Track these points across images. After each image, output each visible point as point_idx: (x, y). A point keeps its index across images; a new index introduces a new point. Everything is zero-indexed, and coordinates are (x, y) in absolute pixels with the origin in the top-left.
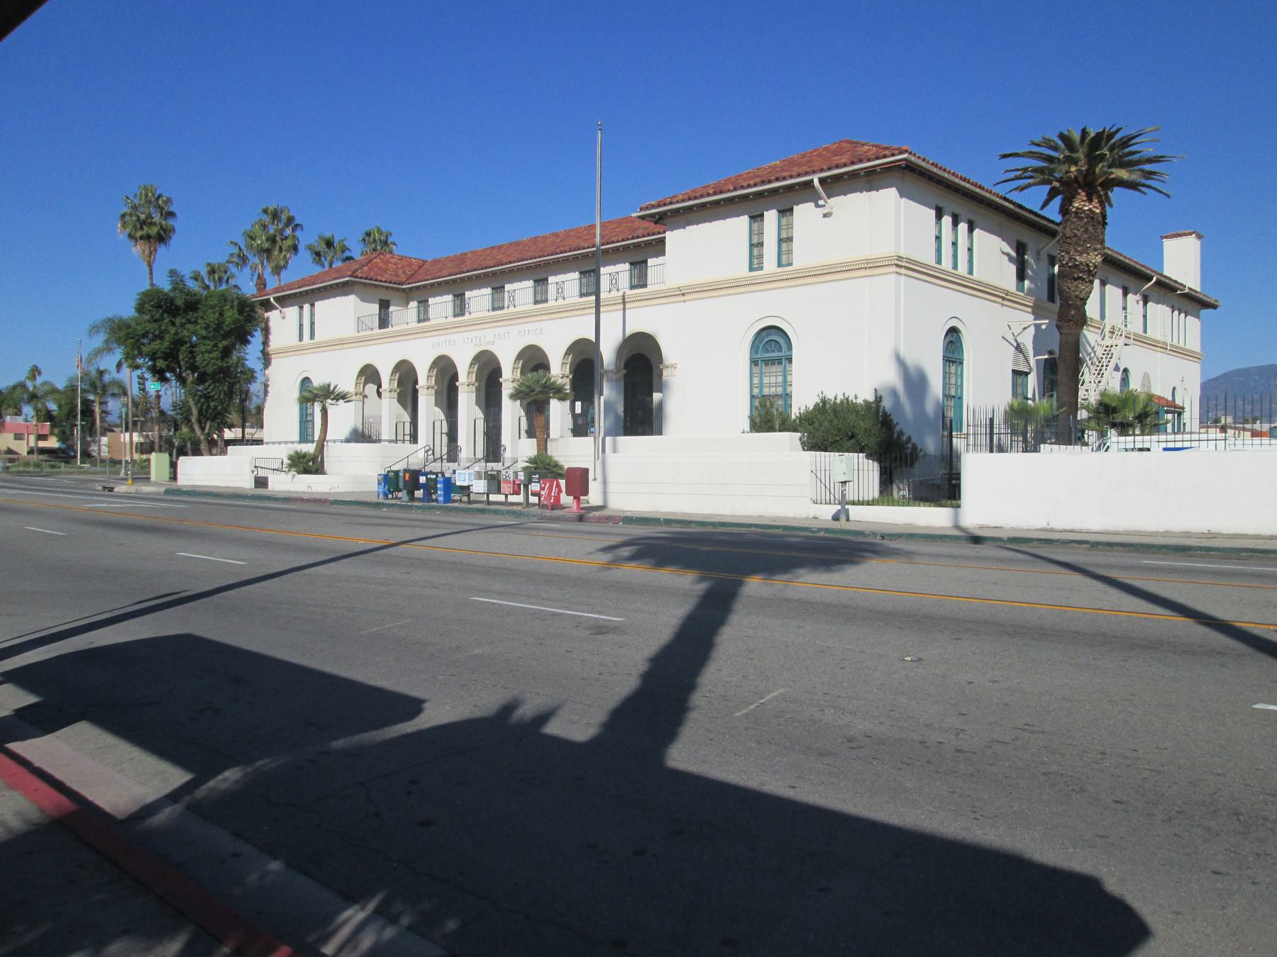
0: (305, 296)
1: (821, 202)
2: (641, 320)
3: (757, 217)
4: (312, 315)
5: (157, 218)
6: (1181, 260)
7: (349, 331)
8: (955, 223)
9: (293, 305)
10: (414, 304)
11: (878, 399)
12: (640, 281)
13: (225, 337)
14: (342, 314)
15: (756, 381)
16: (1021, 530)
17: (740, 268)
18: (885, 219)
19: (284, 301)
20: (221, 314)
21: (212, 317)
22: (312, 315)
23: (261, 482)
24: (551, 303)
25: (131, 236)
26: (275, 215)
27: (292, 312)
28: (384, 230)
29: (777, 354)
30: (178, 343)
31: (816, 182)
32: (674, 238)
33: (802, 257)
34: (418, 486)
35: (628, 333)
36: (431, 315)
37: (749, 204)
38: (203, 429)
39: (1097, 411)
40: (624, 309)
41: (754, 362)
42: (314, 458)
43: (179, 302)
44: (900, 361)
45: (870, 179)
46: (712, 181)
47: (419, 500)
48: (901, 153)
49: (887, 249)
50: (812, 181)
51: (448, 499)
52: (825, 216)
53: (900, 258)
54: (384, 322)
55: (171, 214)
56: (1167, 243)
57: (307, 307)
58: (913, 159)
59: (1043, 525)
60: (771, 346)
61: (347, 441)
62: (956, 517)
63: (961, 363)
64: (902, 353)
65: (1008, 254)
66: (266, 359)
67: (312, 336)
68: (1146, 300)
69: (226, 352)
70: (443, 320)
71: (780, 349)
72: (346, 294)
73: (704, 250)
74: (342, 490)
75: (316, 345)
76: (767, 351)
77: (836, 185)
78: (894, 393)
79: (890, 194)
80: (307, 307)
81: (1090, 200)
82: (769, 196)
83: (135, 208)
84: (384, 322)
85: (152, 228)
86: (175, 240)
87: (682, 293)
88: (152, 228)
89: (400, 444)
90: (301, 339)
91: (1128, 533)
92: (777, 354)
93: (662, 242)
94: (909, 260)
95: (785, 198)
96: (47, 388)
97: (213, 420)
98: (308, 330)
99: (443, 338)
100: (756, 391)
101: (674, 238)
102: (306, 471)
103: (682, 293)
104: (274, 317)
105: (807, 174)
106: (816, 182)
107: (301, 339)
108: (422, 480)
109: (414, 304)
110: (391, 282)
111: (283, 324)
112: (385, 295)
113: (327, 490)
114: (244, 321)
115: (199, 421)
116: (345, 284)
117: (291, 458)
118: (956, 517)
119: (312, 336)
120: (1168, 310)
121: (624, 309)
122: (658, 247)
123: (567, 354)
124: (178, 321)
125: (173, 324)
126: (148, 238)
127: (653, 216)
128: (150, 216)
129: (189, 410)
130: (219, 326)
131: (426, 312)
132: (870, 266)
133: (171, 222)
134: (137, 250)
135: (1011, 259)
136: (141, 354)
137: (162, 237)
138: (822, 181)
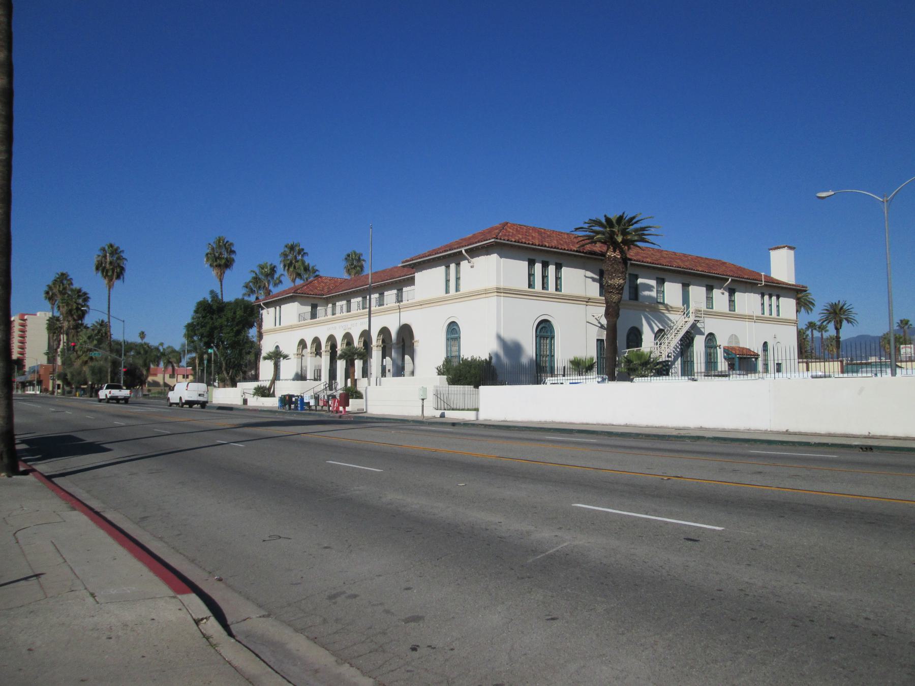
0: (277, 303)
2: (407, 317)
3: (448, 267)
4: (458, 272)
5: (225, 255)
6: (782, 266)
7: (294, 321)
8: (545, 265)
9: (441, 266)
10: (330, 305)
11: (491, 358)
12: (399, 299)
13: (237, 325)
14: (292, 311)
16: (562, 423)
17: (441, 293)
18: (487, 270)
19: (268, 305)
20: (235, 313)
21: (230, 315)
22: (458, 272)
23: (245, 401)
25: (211, 265)
26: (292, 248)
27: (272, 310)
28: (358, 252)
30: (213, 329)
32: (419, 276)
33: (464, 289)
34: (292, 403)
38: (228, 374)
39: (806, 357)
41: (447, 339)
42: (270, 388)
43: (215, 307)
44: (499, 338)
45: (486, 250)
46: (426, 251)
49: (493, 284)
51: (302, 409)
53: (498, 288)
54: (314, 315)
55: (234, 252)
56: (772, 253)
57: (453, 266)
59: (503, 419)
60: (453, 330)
61: (293, 380)
62: (477, 415)
63: (553, 337)
64: (503, 335)
65: (592, 278)
66: (260, 336)
67: (457, 290)
68: (732, 292)
69: (238, 333)
72: (294, 302)
73: (429, 281)
75: (285, 328)
77: (474, 252)
78: (497, 355)
79: (494, 257)
80: (453, 266)
81: (614, 251)
82: (449, 257)
83: (213, 249)
84: (314, 315)
85: (222, 258)
86: (235, 266)
87: (421, 304)
88: (222, 258)
90: (447, 291)
91: (830, 435)
93: (413, 279)
94: (504, 289)
95: (457, 258)
96: (170, 350)
97: (233, 368)
98: (278, 320)
99: (354, 322)
101: (419, 276)
102: (264, 395)
103: (421, 304)
104: (264, 312)
107: (447, 291)
108: (294, 399)
109: (330, 305)
110: (317, 295)
111: (268, 316)
112: (315, 302)
114: (248, 315)
115: (226, 369)
116: (291, 297)
117: (255, 389)
118: (477, 415)
119: (457, 290)
120: (757, 297)
122: (411, 281)
124: (215, 317)
125: (212, 319)
126: (219, 266)
127: (410, 265)
128: (221, 254)
129: (221, 364)
130: (233, 319)
131: (383, 300)
132: (486, 292)
133: (233, 256)
134: (214, 273)
135: (594, 280)
136: (196, 335)
137: (228, 264)
138: (466, 251)
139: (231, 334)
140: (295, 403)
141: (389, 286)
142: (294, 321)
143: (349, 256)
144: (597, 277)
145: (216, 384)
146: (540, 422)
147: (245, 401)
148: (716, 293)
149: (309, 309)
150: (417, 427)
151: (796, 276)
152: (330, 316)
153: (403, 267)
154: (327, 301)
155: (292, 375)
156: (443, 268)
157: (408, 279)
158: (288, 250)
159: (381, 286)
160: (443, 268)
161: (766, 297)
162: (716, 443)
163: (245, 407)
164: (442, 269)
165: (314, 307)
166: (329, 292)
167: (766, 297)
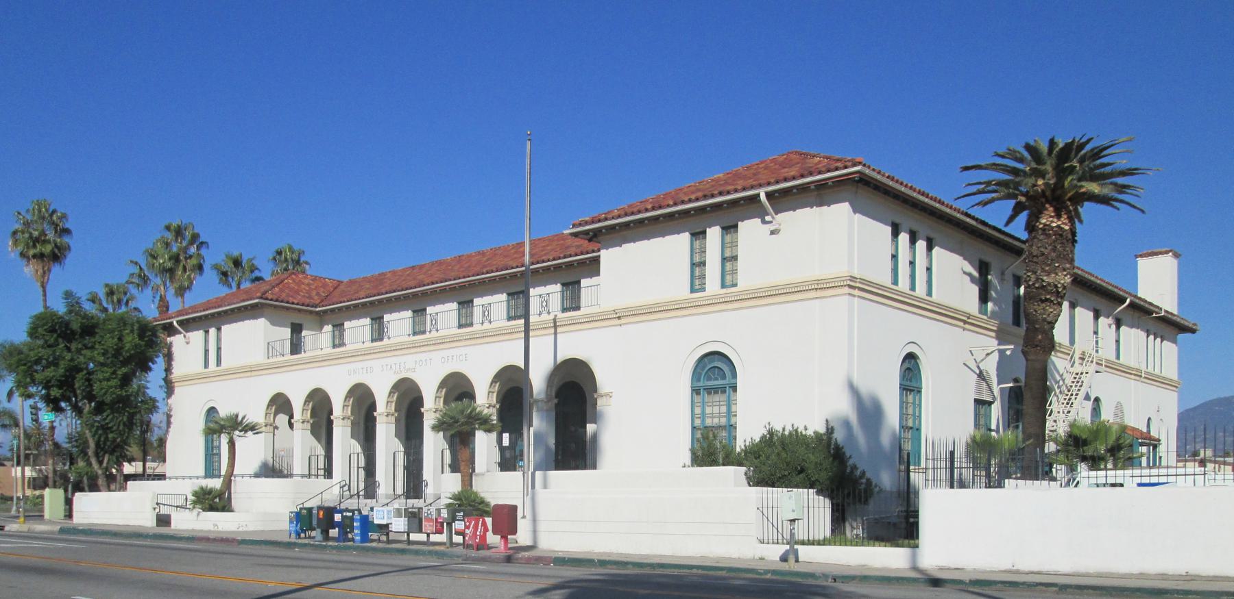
0: (210, 319)
1: (768, 218)
2: (573, 345)
3: (699, 235)
5: (51, 235)
6: (1157, 282)
7: (258, 356)
8: (913, 241)
12: (572, 303)
13: (125, 363)
14: (251, 338)
15: (698, 411)
19: (188, 325)
20: (120, 339)
21: (110, 342)
23: (164, 520)
24: (477, 327)
25: (22, 255)
26: (179, 232)
27: (197, 336)
29: (720, 382)
30: (74, 370)
31: (763, 197)
33: (747, 278)
34: (333, 524)
35: (559, 360)
36: (347, 340)
37: (691, 219)
38: (101, 463)
39: (1066, 444)
40: (556, 334)
41: (696, 391)
43: (75, 326)
44: (853, 390)
47: (334, 539)
48: (855, 165)
49: (839, 269)
50: (758, 195)
51: (365, 538)
52: (772, 233)
53: (853, 278)
54: (296, 348)
55: (67, 231)
56: (1141, 262)
58: (867, 171)
60: (714, 373)
61: (257, 476)
62: (914, 557)
65: (970, 275)
66: (169, 388)
67: (219, 363)
68: (1118, 324)
69: (126, 380)
70: (360, 346)
71: (724, 377)
72: (255, 317)
73: (642, 270)
74: (251, 529)
75: (222, 372)
76: (709, 379)
77: (784, 199)
78: (847, 424)
79: (842, 209)
80: (714, 234)
81: (1059, 216)
82: (712, 211)
84: (296, 348)
86: (70, 259)
87: (618, 316)
89: (313, 479)
90: (206, 365)
92: (720, 382)
93: (596, 260)
94: (863, 281)
95: (730, 214)
100: (698, 422)
101: (609, 257)
103: (618, 316)
104: (177, 341)
105: (752, 187)
106: (763, 197)
107: (206, 365)
108: (338, 517)
110: (304, 305)
111: (187, 350)
112: (297, 319)
113: (234, 529)
114: (145, 346)
115: (97, 455)
118: (914, 557)
119: (219, 363)
120: (1144, 334)
121: (556, 334)
122: (592, 267)
123: (494, 382)
124: (74, 346)
125: (69, 349)
126: (41, 256)
127: (586, 233)
128: (43, 233)
129: (86, 442)
130: (118, 351)
132: (821, 286)
133: (66, 239)
134: (30, 270)
136: (33, 382)
137: (57, 256)
138: (768, 195)
139: (114, 382)
140: (346, 526)
141: (395, 304)
142: (258, 356)
143: (279, 253)
144: (976, 274)
145: (1110, 466)
146: (1099, 575)
147: (164, 520)
148: (1103, 321)
149: (286, 332)
150: (72, 537)
151: (1180, 304)
152: (328, 350)
153: (575, 235)
154: (321, 319)
155: (254, 467)
156: (201, 333)
157: (582, 263)
158: (170, 236)
159: (462, 287)
160: (201, 333)
161: (1152, 337)
162: (263, 547)
163: (163, 530)
164: (680, 242)
165: (296, 329)
166: (322, 302)
167: (1152, 337)
